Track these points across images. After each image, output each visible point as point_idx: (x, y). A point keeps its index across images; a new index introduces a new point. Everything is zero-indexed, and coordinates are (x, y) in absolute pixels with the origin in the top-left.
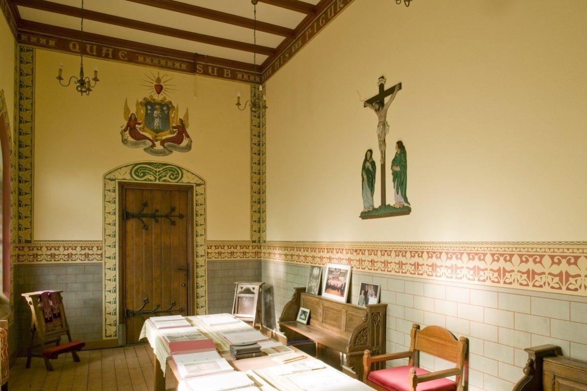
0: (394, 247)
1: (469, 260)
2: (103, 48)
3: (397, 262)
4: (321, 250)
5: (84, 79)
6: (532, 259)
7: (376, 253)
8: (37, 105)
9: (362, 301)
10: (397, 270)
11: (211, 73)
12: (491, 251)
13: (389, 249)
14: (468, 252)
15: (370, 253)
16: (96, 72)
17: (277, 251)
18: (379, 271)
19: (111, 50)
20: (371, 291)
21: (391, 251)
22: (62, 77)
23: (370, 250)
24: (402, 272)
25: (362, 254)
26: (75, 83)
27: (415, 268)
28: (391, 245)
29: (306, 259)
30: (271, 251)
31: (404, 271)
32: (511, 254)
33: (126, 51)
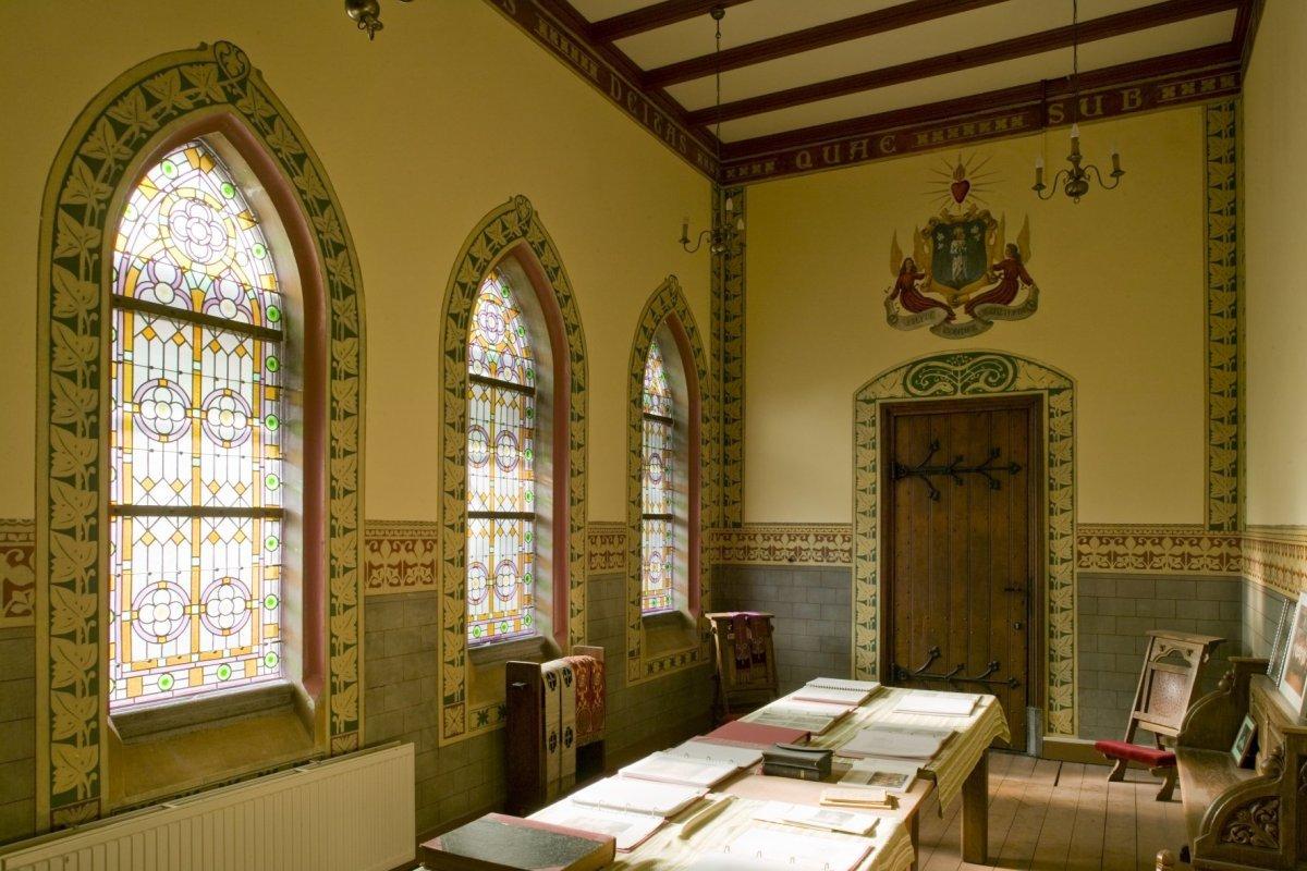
3: (395, 563)
15: (428, 547)
24: (406, 584)
27: (400, 573)
29: (607, 560)
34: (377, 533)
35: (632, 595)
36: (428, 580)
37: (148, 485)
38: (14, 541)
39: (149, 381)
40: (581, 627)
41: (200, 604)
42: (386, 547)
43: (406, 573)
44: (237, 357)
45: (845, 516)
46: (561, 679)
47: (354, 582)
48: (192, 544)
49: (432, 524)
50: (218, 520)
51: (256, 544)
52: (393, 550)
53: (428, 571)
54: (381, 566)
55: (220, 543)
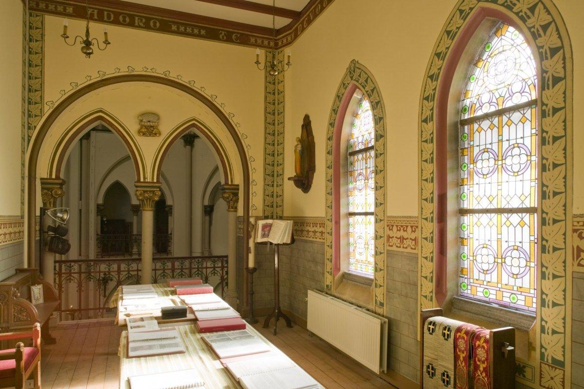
0: (392, 222)
3: (399, 237)
7: (405, 229)
10: (399, 245)
11: (121, 22)
13: (391, 224)
14: (412, 225)
15: (414, 230)
16: (65, 27)
19: (96, 11)
22: (109, 41)
24: (403, 247)
26: (81, 43)
27: (401, 242)
28: (405, 219)
29: (315, 235)
31: (405, 246)
33: (238, 33)
34: (392, 222)
35: (328, 256)
36: (413, 247)
37: (508, 199)
38: (577, 226)
39: (509, 146)
40: (382, 279)
41: (502, 258)
42: (395, 228)
44: (508, 127)
45: (414, 212)
46: (439, 331)
48: (530, 227)
49: (415, 217)
50: (481, 215)
51: (532, 227)
52: (398, 230)
53: (414, 242)
54: (393, 237)
55: (482, 226)
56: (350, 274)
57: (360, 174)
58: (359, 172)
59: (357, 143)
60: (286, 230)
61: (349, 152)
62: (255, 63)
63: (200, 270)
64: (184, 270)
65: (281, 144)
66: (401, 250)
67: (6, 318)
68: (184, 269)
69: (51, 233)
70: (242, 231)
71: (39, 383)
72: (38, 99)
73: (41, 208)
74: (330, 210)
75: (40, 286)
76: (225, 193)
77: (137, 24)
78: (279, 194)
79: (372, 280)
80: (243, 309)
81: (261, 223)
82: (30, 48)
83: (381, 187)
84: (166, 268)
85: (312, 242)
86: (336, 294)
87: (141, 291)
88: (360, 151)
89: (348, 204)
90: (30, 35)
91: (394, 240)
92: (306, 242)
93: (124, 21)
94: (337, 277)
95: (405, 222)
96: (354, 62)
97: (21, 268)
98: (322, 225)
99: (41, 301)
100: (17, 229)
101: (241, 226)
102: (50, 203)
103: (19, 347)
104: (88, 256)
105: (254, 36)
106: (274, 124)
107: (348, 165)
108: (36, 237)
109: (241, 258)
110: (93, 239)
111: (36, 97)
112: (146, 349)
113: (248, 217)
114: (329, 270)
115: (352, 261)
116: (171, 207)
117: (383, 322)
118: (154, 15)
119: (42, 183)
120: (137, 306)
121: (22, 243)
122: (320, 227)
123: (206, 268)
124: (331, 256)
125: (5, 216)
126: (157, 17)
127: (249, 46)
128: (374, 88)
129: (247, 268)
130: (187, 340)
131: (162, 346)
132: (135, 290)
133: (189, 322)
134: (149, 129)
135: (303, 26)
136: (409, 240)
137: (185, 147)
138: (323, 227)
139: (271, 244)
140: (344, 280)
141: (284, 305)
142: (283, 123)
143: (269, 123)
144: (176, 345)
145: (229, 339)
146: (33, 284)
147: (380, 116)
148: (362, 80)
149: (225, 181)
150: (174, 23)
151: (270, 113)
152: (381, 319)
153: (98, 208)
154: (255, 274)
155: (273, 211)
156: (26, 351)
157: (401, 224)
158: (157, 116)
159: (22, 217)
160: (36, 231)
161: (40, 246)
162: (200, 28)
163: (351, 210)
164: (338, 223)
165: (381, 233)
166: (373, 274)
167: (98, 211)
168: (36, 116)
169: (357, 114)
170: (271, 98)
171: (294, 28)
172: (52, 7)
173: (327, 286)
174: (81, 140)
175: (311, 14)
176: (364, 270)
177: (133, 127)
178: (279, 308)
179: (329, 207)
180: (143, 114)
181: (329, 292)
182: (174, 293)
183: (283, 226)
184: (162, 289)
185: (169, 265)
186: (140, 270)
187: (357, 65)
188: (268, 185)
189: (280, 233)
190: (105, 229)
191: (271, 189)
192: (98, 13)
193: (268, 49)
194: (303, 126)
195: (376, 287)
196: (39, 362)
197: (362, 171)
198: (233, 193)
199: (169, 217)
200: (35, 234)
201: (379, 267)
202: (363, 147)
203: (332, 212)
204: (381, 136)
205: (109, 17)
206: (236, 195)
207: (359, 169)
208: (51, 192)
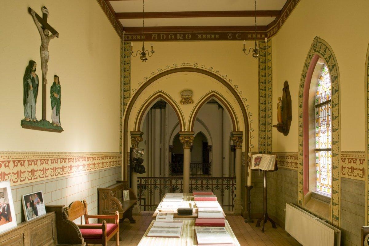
1: (29, 165)
2: (153, 35)
3: (350, 167)
4: (70, 160)
5: (144, 52)
6: (4, 164)
8: (132, 67)
9: (31, 214)
12: (13, 158)
14: (40, 159)
15: (361, 162)
17: (81, 163)
18: (39, 179)
19: (156, 35)
20: (36, 199)
21: (48, 160)
22: (154, 50)
23: (30, 160)
24: (353, 176)
25: (21, 165)
30: (71, 164)
31: (355, 175)
32: (9, 161)
33: (240, 33)
36: (361, 176)
42: (347, 161)
43: (45, 172)
47: (338, 172)
49: (363, 152)
52: (349, 162)
53: (362, 172)
54: (345, 167)
56: (316, 194)
57: (324, 120)
58: (323, 119)
59: (321, 98)
60: (271, 161)
61: (315, 105)
62: (243, 50)
63: (228, 186)
64: (157, 185)
65: (270, 102)
66: (352, 177)
67: (107, 207)
68: (219, 185)
69: (135, 162)
70: (244, 161)
71: (118, 244)
72: (128, 88)
73: (131, 148)
74: (301, 147)
75: (128, 191)
76: (233, 137)
77: (178, 38)
78: (269, 137)
79: (330, 199)
80: (245, 213)
81: (254, 156)
82: (124, 61)
83: (336, 130)
84: (218, 184)
85: (290, 170)
86: (306, 208)
87: (175, 197)
88: (324, 103)
89: (315, 143)
90: (124, 55)
91: (347, 170)
92: (286, 170)
93: (171, 38)
94: (306, 196)
95: (355, 156)
96: (317, 38)
97: (120, 180)
98: (296, 158)
99: (128, 199)
100: (117, 160)
101: (244, 158)
102: (135, 145)
103: (104, 223)
104: (165, 175)
105: (250, 33)
106: (265, 90)
107: (315, 114)
108: (127, 164)
109: (244, 180)
110: (167, 165)
111: (127, 87)
112: (158, 233)
113: (248, 152)
114: (301, 190)
115: (318, 184)
116: (211, 147)
117: (336, 231)
118: (187, 31)
119: (131, 134)
120: (168, 206)
121: (121, 167)
122: (291, 159)
123: (212, 185)
124: (302, 180)
125: (110, 153)
126: (189, 32)
127: (247, 40)
128: (331, 56)
129: (247, 186)
130: (185, 229)
131: (168, 232)
132: (172, 196)
133: (193, 219)
134: (187, 100)
135: (283, 20)
136: (358, 170)
137: (219, 109)
138: (297, 159)
139: (261, 170)
140: (312, 198)
141: (271, 212)
142: (271, 88)
143: (261, 90)
144: (176, 232)
145: (210, 232)
146: (124, 190)
147: (335, 76)
148: (322, 51)
149: (234, 129)
150: (200, 34)
151: (262, 83)
152: (334, 230)
153: (170, 147)
154: (252, 191)
155: (265, 148)
156: (109, 226)
157: (44, 159)
158: (191, 91)
159: (121, 153)
160: (127, 160)
161: (130, 169)
162: (215, 34)
163: (318, 147)
164: (307, 156)
165: (336, 164)
166: (331, 194)
167: (170, 149)
168: (127, 98)
169: (321, 77)
170: (262, 72)
171: (277, 22)
172: (134, 37)
173: (300, 201)
174: (151, 109)
175: (288, 11)
176: (327, 191)
177: (177, 99)
178: (267, 214)
179: (300, 145)
180: (183, 91)
181: (301, 206)
182: (193, 199)
183: (269, 159)
184: (188, 197)
185: (200, 182)
186: (183, 185)
187: (319, 40)
188: (262, 131)
189: (267, 163)
190: (174, 160)
191: (263, 133)
192: (158, 36)
193: (259, 40)
194: (283, 89)
195: (333, 205)
196: (118, 233)
197: (324, 118)
198: (239, 137)
199: (210, 153)
200: (127, 162)
201: (335, 189)
202: (325, 100)
203: (302, 148)
204: (336, 91)
205: (163, 37)
206: (241, 138)
207: (323, 116)
208: (136, 139)
